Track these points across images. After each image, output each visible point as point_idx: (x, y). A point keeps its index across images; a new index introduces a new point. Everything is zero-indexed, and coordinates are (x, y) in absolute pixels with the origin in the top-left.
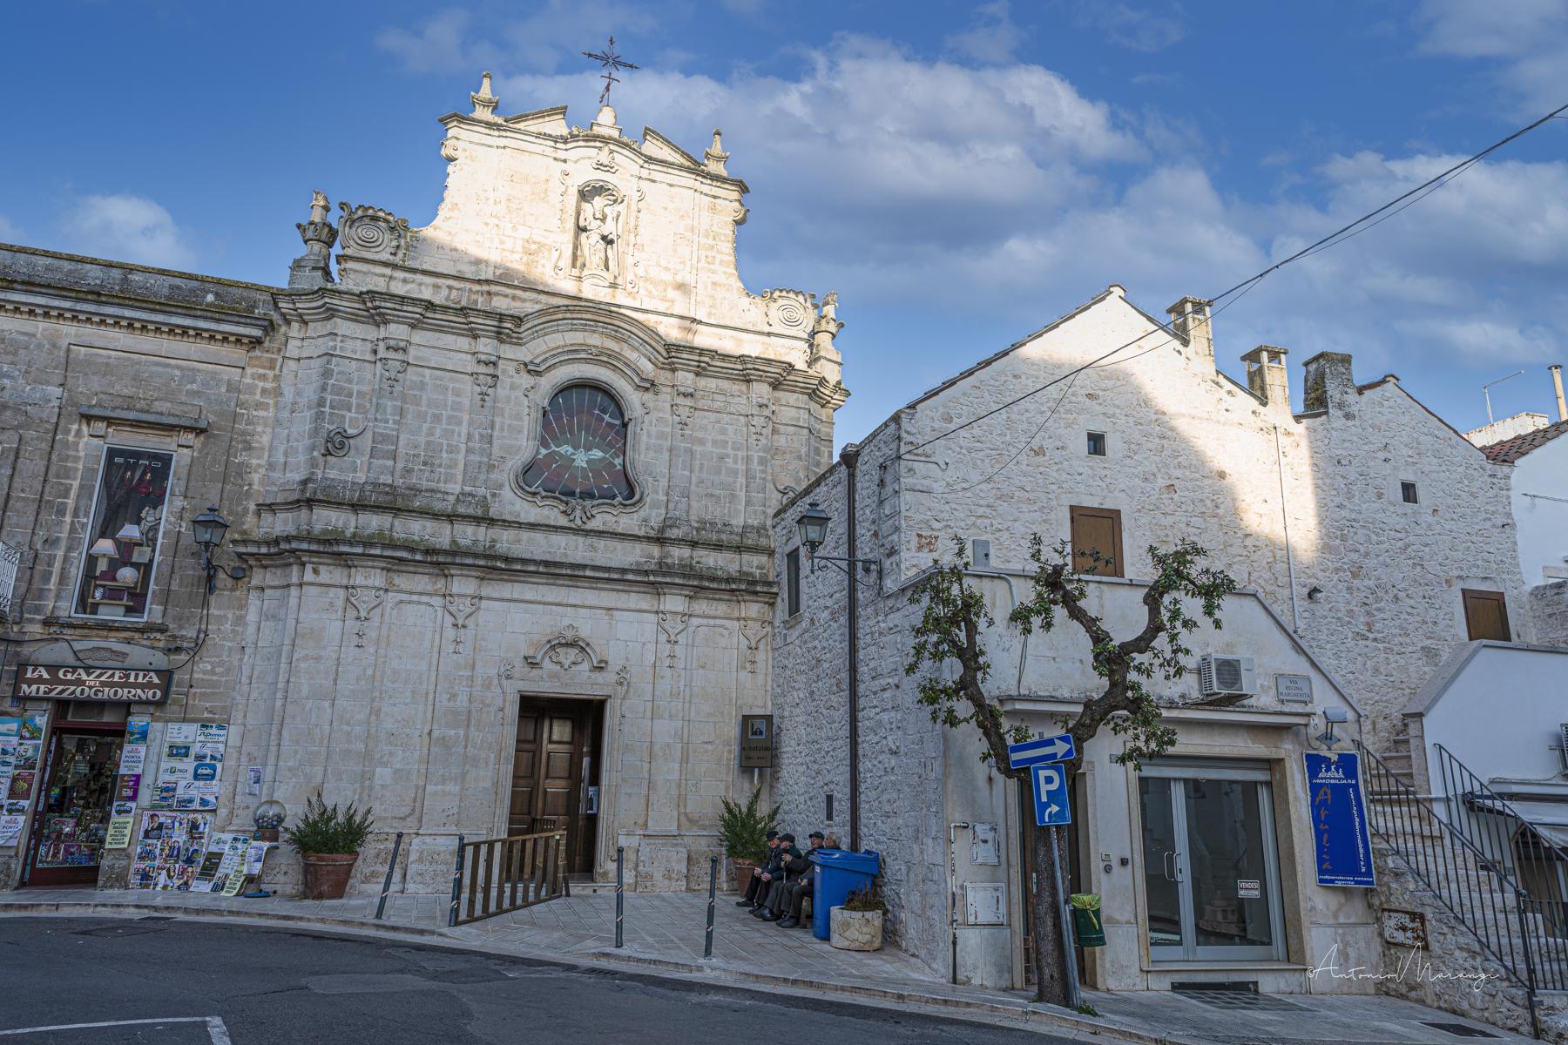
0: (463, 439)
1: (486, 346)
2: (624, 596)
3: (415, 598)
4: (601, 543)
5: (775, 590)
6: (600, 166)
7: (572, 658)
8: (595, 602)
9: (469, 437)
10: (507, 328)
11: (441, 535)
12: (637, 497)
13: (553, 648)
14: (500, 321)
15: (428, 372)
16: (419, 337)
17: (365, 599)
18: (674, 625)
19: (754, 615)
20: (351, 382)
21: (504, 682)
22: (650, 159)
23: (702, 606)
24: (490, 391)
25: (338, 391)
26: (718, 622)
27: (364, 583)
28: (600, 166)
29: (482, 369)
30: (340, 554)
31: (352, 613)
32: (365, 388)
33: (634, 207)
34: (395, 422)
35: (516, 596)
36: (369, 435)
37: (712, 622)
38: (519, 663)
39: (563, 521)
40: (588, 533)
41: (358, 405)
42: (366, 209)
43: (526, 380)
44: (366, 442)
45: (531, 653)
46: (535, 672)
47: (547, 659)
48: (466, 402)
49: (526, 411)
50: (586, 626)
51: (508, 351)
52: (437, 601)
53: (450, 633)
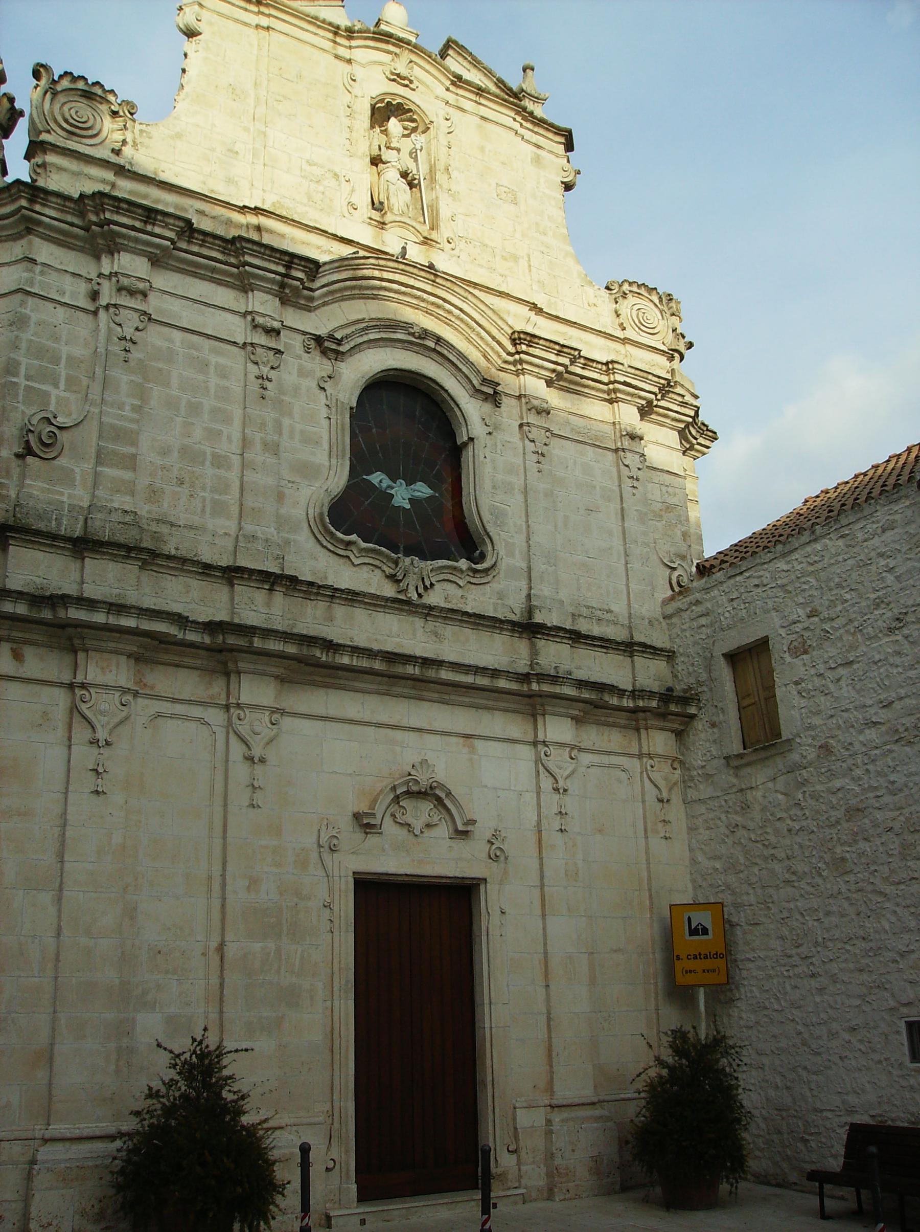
0: (235, 447)
1: (263, 303)
2: (486, 716)
3: (179, 709)
4: (449, 630)
5: (692, 710)
6: (397, 78)
7: (424, 819)
8: (448, 727)
9: (246, 443)
10: (296, 277)
11: (204, 602)
12: (485, 565)
13: (397, 799)
14: (288, 267)
15: (177, 335)
16: (164, 280)
17: (103, 706)
18: (558, 759)
19: (660, 750)
20: (57, 339)
21: (327, 857)
22: (458, 81)
23: (592, 736)
24: (273, 374)
25: (39, 352)
26: (615, 760)
27: (100, 679)
28: (397, 78)
29: (260, 338)
30: (63, 626)
31: (81, 734)
32: (79, 351)
33: (443, 140)
34: (135, 409)
35: (332, 712)
36: (94, 426)
37: (606, 759)
38: (345, 824)
39: (389, 590)
40: (429, 612)
41: (69, 379)
42: (75, 79)
43: (319, 365)
44: (89, 437)
45: (363, 808)
46: (373, 840)
47: (388, 820)
48: (236, 388)
49: (324, 412)
50: (444, 763)
51: (293, 318)
52: (216, 717)
53: (240, 772)
